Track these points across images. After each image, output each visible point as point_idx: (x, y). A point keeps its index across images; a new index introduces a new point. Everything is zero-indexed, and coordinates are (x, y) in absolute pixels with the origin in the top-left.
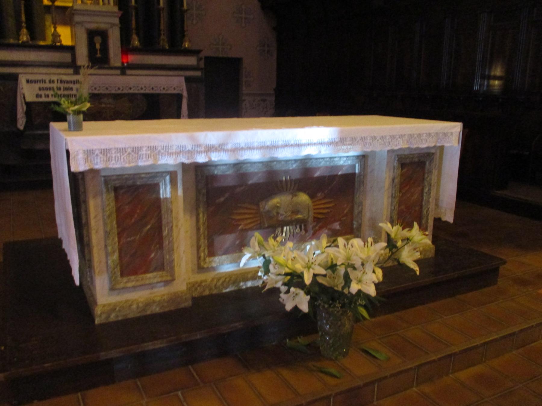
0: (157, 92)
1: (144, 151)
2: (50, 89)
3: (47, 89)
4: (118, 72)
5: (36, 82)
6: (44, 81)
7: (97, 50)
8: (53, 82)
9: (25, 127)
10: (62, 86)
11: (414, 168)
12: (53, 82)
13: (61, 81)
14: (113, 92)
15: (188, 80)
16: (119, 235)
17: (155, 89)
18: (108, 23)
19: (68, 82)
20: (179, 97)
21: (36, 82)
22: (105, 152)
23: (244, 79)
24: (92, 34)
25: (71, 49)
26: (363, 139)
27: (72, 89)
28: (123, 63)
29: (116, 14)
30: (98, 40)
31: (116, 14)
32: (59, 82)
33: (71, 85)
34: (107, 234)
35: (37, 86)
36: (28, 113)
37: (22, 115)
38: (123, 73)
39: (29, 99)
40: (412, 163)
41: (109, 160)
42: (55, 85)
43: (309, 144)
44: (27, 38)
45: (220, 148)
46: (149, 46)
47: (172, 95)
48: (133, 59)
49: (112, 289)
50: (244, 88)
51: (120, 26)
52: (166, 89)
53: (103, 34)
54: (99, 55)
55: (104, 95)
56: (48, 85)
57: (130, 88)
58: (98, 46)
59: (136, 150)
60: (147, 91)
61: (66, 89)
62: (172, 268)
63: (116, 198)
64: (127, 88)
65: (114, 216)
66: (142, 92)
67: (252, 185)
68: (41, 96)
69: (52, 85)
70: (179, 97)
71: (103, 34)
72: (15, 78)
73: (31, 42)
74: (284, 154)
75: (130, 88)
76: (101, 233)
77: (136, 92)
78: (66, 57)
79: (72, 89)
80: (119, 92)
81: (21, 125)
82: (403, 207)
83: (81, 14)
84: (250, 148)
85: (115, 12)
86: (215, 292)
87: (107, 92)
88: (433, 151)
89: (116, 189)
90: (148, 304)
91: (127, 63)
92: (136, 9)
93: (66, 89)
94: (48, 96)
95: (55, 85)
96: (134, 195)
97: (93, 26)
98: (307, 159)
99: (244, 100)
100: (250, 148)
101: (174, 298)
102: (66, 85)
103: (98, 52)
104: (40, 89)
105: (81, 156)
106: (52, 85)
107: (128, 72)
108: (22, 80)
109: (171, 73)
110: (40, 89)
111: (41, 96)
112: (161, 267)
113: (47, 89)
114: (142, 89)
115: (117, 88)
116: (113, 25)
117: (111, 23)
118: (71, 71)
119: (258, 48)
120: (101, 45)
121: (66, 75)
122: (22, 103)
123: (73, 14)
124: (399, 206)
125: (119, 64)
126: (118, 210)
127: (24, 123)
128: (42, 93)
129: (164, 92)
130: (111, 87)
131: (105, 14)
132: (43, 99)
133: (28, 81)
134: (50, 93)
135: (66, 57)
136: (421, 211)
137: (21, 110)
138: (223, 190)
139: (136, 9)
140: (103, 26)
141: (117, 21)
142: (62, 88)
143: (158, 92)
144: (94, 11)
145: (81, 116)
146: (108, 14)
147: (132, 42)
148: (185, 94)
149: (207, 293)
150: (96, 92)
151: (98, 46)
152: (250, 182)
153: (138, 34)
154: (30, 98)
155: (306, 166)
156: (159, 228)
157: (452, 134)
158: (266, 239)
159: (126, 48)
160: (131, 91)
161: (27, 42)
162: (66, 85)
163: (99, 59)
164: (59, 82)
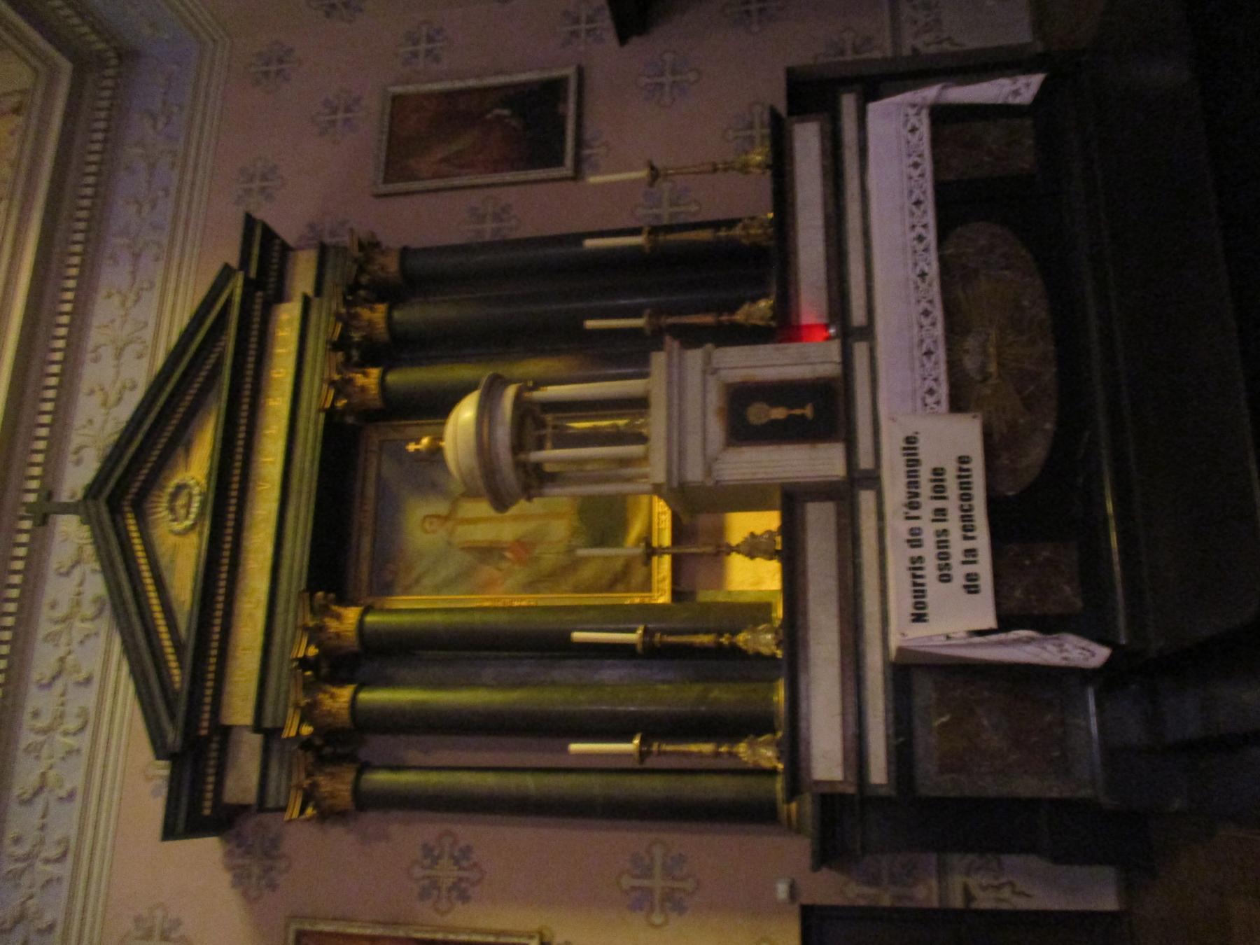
0: (928, 185)
3: (943, 556)
5: (919, 593)
6: (916, 565)
7: (790, 418)
8: (915, 532)
9: (1102, 641)
10: (928, 506)
12: (915, 532)
14: (939, 331)
17: (917, 194)
18: (704, 383)
19: (913, 483)
20: (941, 115)
21: (919, 593)
23: (849, 57)
24: (741, 432)
27: (938, 472)
29: (675, 360)
30: (759, 413)
31: (675, 360)
32: (914, 513)
33: (925, 474)
36: (1048, 625)
37: (1050, 647)
38: (867, 333)
42: (929, 531)
44: (766, 744)
48: (811, 305)
50: (877, 54)
51: (709, 346)
52: (915, 159)
53: (740, 397)
54: (808, 411)
55: (953, 366)
56: (929, 550)
57: (923, 275)
58: (779, 413)
60: (930, 219)
61: (939, 491)
64: (923, 286)
66: (931, 236)
68: (971, 577)
69: (929, 539)
70: (941, 115)
71: (740, 397)
72: (906, 671)
73: (780, 734)
75: (923, 275)
77: (933, 256)
78: (820, 517)
79: (938, 472)
80: (938, 313)
81: (1093, 655)
83: (681, 467)
85: (670, 358)
87: (941, 354)
91: (827, 327)
92: (658, 311)
93: (939, 491)
94: (971, 552)
95: (929, 531)
97: (716, 429)
99: (915, 50)
102: (926, 488)
103: (798, 412)
104: (945, 578)
106: (929, 539)
107: (858, 316)
110: (945, 578)
111: (971, 577)
113: (943, 556)
114: (920, 238)
115: (926, 322)
116: (709, 370)
117: (704, 372)
118: (866, 499)
119: (755, 28)
120: (774, 403)
122: (1002, 643)
123: (682, 485)
125: (834, 348)
127: (1085, 643)
128: (959, 572)
129: (927, 165)
130: (922, 341)
131: (675, 370)
132: (984, 568)
133: (919, 618)
134: (957, 546)
137: (1031, 649)
139: (658, 311)
140: (715, 399)
141: (695, 357)
142: (939, 504)
144: (669, 417)
146: (675, 377)
147: (761, 323)
148: (930, 93)
150: (943, 390)
151: (779, 413)
153: (733, 309)
154: (981, 611)
158: (1061, 646)
159: (783, 328)
160: (933, 269)
161: (778, 744)
162: (926, 488)
163: (823, 410)
164: (914, 513)
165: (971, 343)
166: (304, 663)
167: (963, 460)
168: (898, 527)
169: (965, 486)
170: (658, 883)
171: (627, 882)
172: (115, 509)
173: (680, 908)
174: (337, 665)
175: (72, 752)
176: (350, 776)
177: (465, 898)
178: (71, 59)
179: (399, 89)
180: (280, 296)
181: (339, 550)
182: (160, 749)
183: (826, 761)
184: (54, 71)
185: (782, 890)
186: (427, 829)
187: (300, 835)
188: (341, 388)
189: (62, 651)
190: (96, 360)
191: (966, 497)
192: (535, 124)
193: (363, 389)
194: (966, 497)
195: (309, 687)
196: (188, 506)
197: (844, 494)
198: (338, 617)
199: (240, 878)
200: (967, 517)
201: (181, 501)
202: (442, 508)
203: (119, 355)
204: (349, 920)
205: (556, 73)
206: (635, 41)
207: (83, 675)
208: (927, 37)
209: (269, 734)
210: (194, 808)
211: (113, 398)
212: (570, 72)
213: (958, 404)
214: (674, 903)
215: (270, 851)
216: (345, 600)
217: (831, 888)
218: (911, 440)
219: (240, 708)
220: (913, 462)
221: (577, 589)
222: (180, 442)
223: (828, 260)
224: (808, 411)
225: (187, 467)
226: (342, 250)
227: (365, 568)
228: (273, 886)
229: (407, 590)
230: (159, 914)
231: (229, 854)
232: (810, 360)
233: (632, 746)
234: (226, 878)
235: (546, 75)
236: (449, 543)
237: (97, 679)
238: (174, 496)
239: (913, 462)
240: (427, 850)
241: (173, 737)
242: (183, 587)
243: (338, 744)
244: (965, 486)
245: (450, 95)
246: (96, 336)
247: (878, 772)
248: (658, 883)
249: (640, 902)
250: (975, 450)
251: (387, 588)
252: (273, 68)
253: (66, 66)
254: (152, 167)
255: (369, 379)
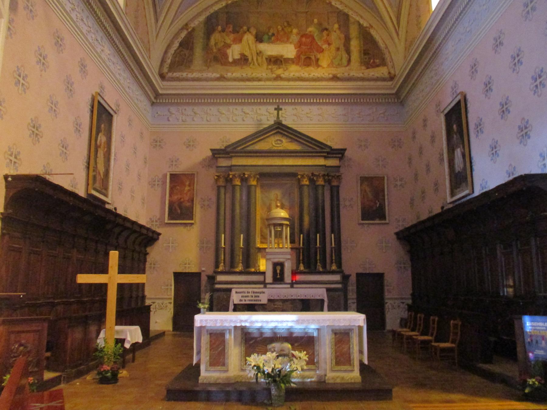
1: (218, 321)
2: (247, 296)
3: (245, 297)
4: (289, 286)
5: (240, 293)
10: (253, 295)
11: (342, 336)
13: (254, 292)
14: (282, 298)
15: (328, 290)
16: (210, 350)
19: (257, 293)
20: (322, 301)
21: (240, 293)
22: (206, 320)
24: (275, 265)
25: (263, 273)
26: (318, 320)
28: (292, 281)
30: (278, 268)
33: (258, 294)
34: (206, 349)
35: (240, 295)
38: (292, 287)
39: (236, 302)
40: (341, 333)
41: (207, 323)
42: (250, 295)
43: (272, 322)
45: (246, 321)
46: (311, 269)
47: (318, 300)
48: (299, 278)
49: (206, 370)
50: (386, 294)
54: (278, 277)
55: (277, 300)
56: (246, 294)
58: (278, 271)
59: (216, 320)
60: (302, 298)
61: (256, 296)
62: (228, 366)
63: (211, 337)
65: (209, 343)
66: (299, 298)
67: (265, 338)
69: (248, 295)
70: (322, 301)
71: (282, 265)
74: (280, 325)
76: (204, 349)
77: (296, 298)
79: (259, 296)
80: (285, 298)
82: (338, 354)
84: (257, 322)
86: (247, 381)
87: (278, 298)
88: (353, 328)
89: (210, 334)
90: (218, 378)
93: (256, 296)
95: (250, 295)
96: (217, 337)
97: (276, 260)
98: (275, 328)
99: (386, 303)
100: (257, 322)
101: (228, 378)
102: (256, 294)
104: (242, 296)
105: (199, 321)
106: (248, 295)
107: (295, 286)
108: (234, 291)
109: (314, 286)
110: (242, 296)
112: (224, 365)
113: (245, 297)
118: (262, 286)
119: (396, 266)
120: (280, 271)
121: (258, 288)
124: (336, 353)
125: (290, 282)
126: (211, 341)
128: (243, 299)
132: (243, 302)
133: (236, 292)
134: (247, 299)
135: (260, 278)
136: (350, 357)
138: (253, 338)
140: (281, 260)
143: (309, 298)
145: (205, 310)
148: (326, 299)
149: (244, 380)
151: (278, 271)
152: (264, 336)
153: (303, 263)
155: (290, 332)
156: (224, 349)
157: (359, 320)
160: (293, 298)
162: (256, 294)
165: (281, 303)
166: (244, 174)
167: (260, 300)
168: (250, 290)
169: (256, 300)
170: (205, 245)
171: (205, 239)
172: (277, 128)
173: (200, 249)
174: (244, 180)
175: (228, 119)
176: (223, 185)
177: (202, 207)
178: (396, 92)
179: (386, 178)
180: (325, 157)
181: (268, 177)
182: (226, 147)
183: (220, 278)
184: (393, 89)
185: (203, 269)
186: (214, 199)
187: (213, 172)
188: (303, 176)
189: (250, 113)
190: (318, 109)
191: (255, 300)
192: (374, 212)
193: (303, 181)
194: (255, 300)
195: (239, 176)
196: (278, 144)
197: (264, 283)
198: (253, 181)
199: (204, 160)
200: (251, 300)
201: (279, 142)
202: (279, 198)
203: (319, 115)
204: (197, 185)
205: (387, 217)
206: (395, 237)
207: (245, 119)
208: (390, 307)
209: (230, 168)
210: (216, 153)
211: (309, 115)
212: (387, 221)
213: (269, 300)
214: (201, 248)
215: (210, 166)
216: (258, 180)
217: (204, 279)
218: (264, 293)
219: (236, 161)
220: (260, 293)
221: (261, 228)
222: (293, 140)
223: (311, 281)
224: (278, 277)
225: (287, 142)
226: (339, 171)
227: (267, 182)
228: (203, 167)
229: (261, 192)
230: (187, 259)
231: (209, 157)
232: (288, 277)
233: (223, 246)
234: (204, 157)
235: (387, 215)
236: (271, 200)
237: (244, 123)
238: (280, 140)
239: (260, 293)
240: (210, 199)
241: (229, 149)
242: (259, 147)
243: (229, 180)
244: (256, 300)
245: (383, 191)
246: (324, 108)
247: (217, 286)
248: (205, 245)
249: (202, 242)
250: (262, 302)
251: (262, 187)
252: (396, 144)
253: (394, 92)
254: (369, 115)
255: (306, 182)
